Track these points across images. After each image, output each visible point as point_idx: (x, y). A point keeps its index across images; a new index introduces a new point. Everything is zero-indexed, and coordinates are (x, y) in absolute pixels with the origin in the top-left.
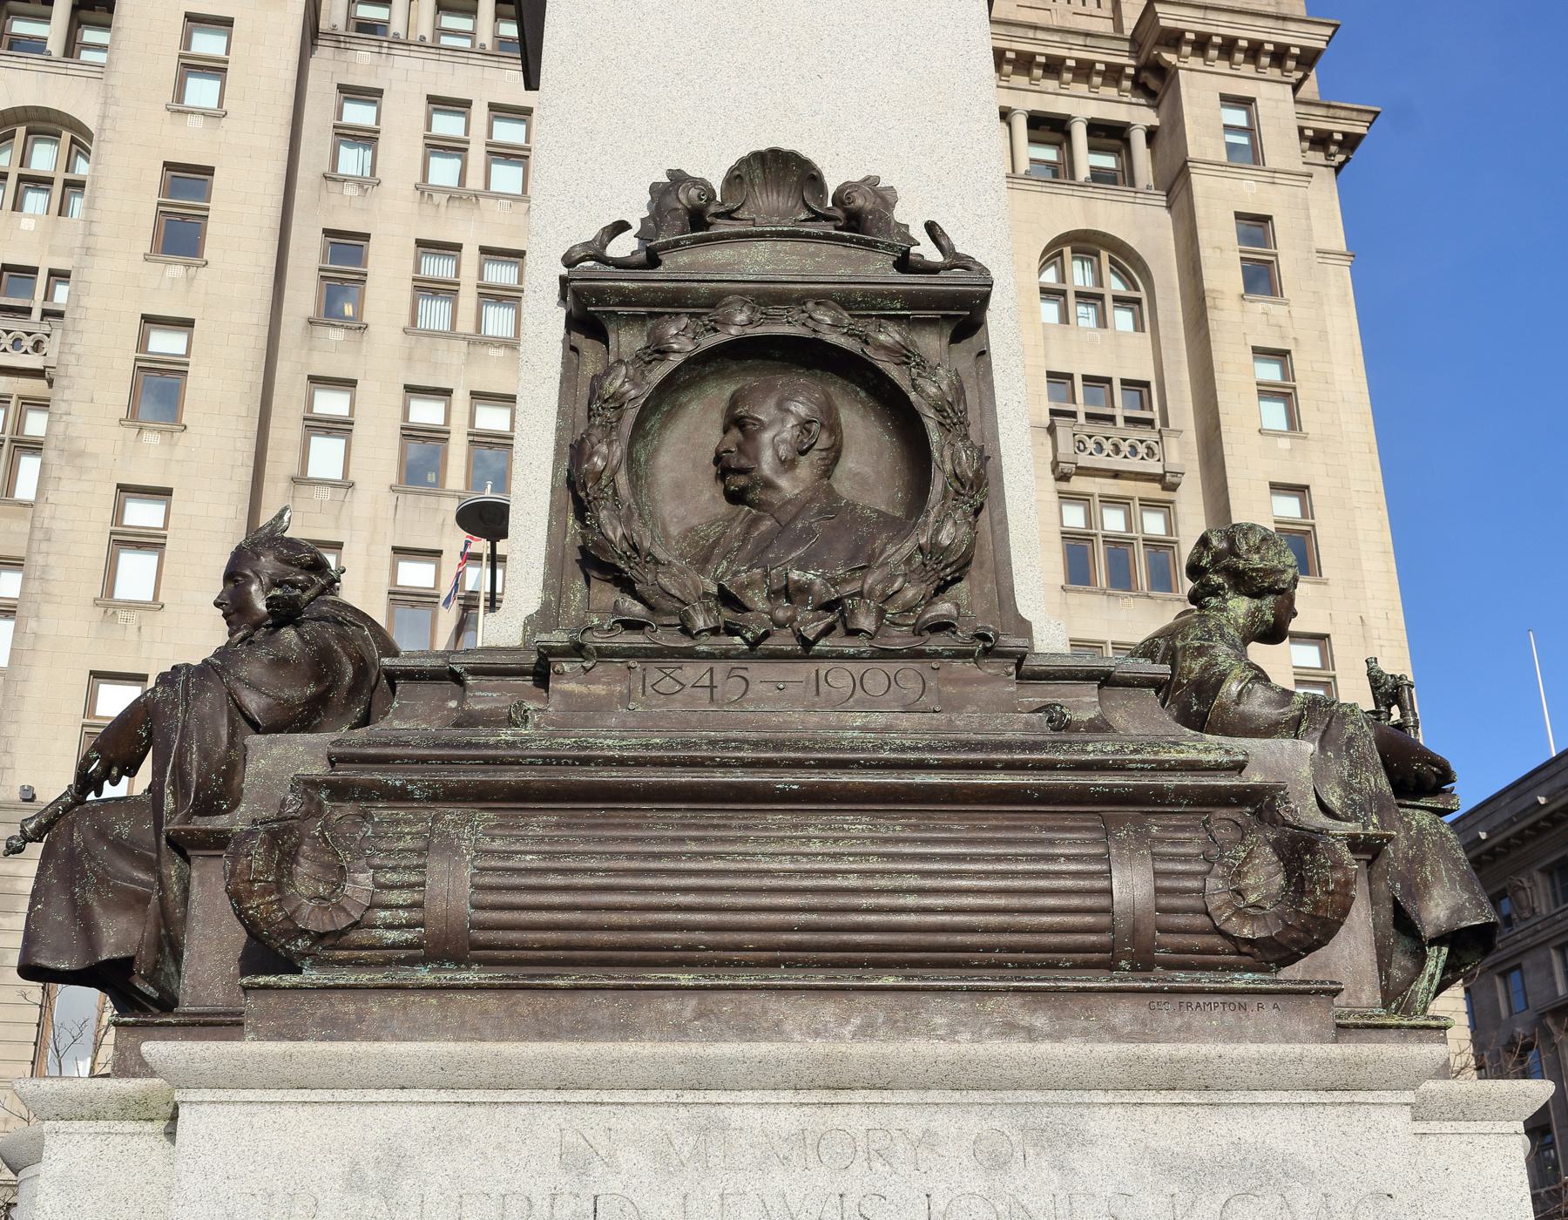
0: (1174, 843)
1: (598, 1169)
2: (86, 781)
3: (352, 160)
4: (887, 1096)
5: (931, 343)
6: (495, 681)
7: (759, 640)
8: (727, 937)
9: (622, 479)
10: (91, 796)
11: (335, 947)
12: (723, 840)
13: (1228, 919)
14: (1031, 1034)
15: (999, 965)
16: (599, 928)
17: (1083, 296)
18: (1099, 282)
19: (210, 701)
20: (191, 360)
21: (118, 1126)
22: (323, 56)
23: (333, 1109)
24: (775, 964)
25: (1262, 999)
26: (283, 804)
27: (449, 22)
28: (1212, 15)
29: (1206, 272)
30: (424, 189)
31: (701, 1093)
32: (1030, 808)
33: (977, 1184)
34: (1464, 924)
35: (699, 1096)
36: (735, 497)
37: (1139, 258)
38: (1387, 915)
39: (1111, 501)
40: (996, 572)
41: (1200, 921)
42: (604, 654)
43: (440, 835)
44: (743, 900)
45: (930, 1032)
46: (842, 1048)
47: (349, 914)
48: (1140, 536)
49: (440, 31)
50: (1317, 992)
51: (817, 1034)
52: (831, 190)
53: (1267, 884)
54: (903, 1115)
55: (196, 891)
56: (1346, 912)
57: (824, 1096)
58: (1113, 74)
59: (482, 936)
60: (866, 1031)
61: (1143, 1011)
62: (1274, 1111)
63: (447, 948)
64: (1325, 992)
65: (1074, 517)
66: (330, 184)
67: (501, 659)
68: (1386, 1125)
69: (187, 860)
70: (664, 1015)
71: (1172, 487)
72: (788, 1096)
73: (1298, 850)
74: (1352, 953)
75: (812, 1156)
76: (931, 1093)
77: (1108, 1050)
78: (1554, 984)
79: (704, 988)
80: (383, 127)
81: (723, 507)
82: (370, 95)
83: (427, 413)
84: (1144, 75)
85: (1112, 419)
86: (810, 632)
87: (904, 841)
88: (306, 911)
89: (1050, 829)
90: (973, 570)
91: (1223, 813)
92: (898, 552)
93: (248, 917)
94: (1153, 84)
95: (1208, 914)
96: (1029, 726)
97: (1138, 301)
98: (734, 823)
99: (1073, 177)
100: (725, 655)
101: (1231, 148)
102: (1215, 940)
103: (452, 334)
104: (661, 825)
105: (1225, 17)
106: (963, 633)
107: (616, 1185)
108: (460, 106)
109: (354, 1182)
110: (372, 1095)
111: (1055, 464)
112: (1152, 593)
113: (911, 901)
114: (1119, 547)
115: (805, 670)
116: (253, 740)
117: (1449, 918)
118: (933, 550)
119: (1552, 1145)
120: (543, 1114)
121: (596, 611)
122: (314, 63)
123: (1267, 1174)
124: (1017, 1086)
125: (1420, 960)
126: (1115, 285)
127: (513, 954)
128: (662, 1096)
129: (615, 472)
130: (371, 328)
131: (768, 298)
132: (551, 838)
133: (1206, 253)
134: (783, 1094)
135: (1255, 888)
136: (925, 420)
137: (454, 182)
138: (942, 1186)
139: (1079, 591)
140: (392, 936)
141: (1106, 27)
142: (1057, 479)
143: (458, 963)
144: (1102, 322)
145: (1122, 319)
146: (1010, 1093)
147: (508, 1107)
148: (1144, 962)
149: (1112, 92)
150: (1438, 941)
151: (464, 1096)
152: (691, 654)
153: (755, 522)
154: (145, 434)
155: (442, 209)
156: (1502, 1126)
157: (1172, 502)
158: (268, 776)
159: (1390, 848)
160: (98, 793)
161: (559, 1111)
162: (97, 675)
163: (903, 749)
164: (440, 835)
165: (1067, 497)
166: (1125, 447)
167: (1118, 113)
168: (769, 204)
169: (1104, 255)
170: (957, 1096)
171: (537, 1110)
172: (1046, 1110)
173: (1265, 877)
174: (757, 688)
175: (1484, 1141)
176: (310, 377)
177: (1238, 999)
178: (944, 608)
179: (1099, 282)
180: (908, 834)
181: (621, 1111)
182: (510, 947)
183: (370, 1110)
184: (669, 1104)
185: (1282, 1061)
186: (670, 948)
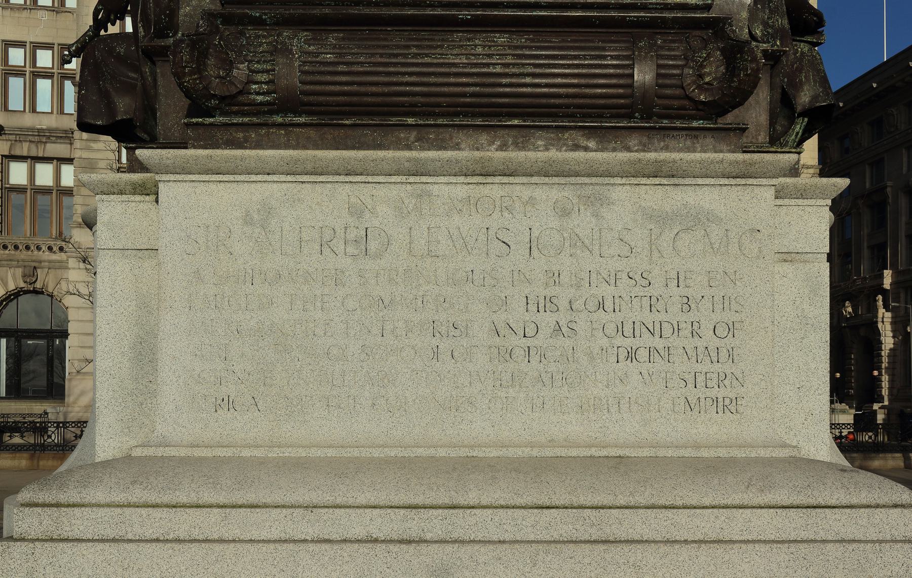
0: (670, 49)
1: (367, 215)
2: (99, 24)
4: (511, 179)
8: (433, 100)
10: (102, 33)
11: (230, 105)
12: (431, 47)
13: (694, 90)
14: (586, 149)
16: (366, 94)
21: (132, 198)
23: (234, 185)
24: (457, 114)
25: (706, 133)
26: (198, 26)
31: (418, 178)
32: (594, 30)
34: (818, 104)
38: (778, 96)
41: (678, 92)
43: (281, 43)
45: (536, 149)
46: (489, 154)
47: (236, 86)
50: (735, 129)
51: (478, 149)
53: (716, 72)
54: (520, 189)
55: (160, 82)
56: (755, 86)
59: (305, 99)
60: (503, 147)
61: (645, 140)
62: (706, 188)
63: (288, 104)
64: (740, 129)
68: (761, 195)
69: (154, 63)
70: (400, 139)
72: (462, 179)
73: (735, 51)
74: (757, 112)
75: (473, 209)
76: (534, 178)
77: (623, 156)
78: (865, 183)
79: (420, 125)
87: (526, 47)
88: (214, 85)
89: (603, 41)
91: (697, 33)
93: (185, 87)
95: (683, 88)
98: (436, 37)
102: (686, 102)
107: (376, 223)
109: (248, 220)
110: (254, 178)
113: (528, 80)
117: (810, 102)
119: (850, 262)
120: (340, 188)
123: (697, 220)
124: (577, 174)
125: (792, 122)
127: (323, 108)
132: (340, 45)
134: (459, 178)
135: (709, 74)
138: (538, 224)
140: (260, 98)
146: (573, 178)
147: (321, 184)
148: (648, 115)
150: (803, 114)
156: (821, 202)
159: (784, 59)
160: (106, 31)
161: (347, 186)
164: (281, 43)
170: (547, 180)
171: (336, 185)
172: (591, 187)
173: (714, 70)
175: (809, 209)
177: (694, 133)
180: (528, 43)
181: (377, 186)
182: (320, 104)
183: (253, 185)
184: (402, 183)
185: (712, 162)
186: (403, 106)
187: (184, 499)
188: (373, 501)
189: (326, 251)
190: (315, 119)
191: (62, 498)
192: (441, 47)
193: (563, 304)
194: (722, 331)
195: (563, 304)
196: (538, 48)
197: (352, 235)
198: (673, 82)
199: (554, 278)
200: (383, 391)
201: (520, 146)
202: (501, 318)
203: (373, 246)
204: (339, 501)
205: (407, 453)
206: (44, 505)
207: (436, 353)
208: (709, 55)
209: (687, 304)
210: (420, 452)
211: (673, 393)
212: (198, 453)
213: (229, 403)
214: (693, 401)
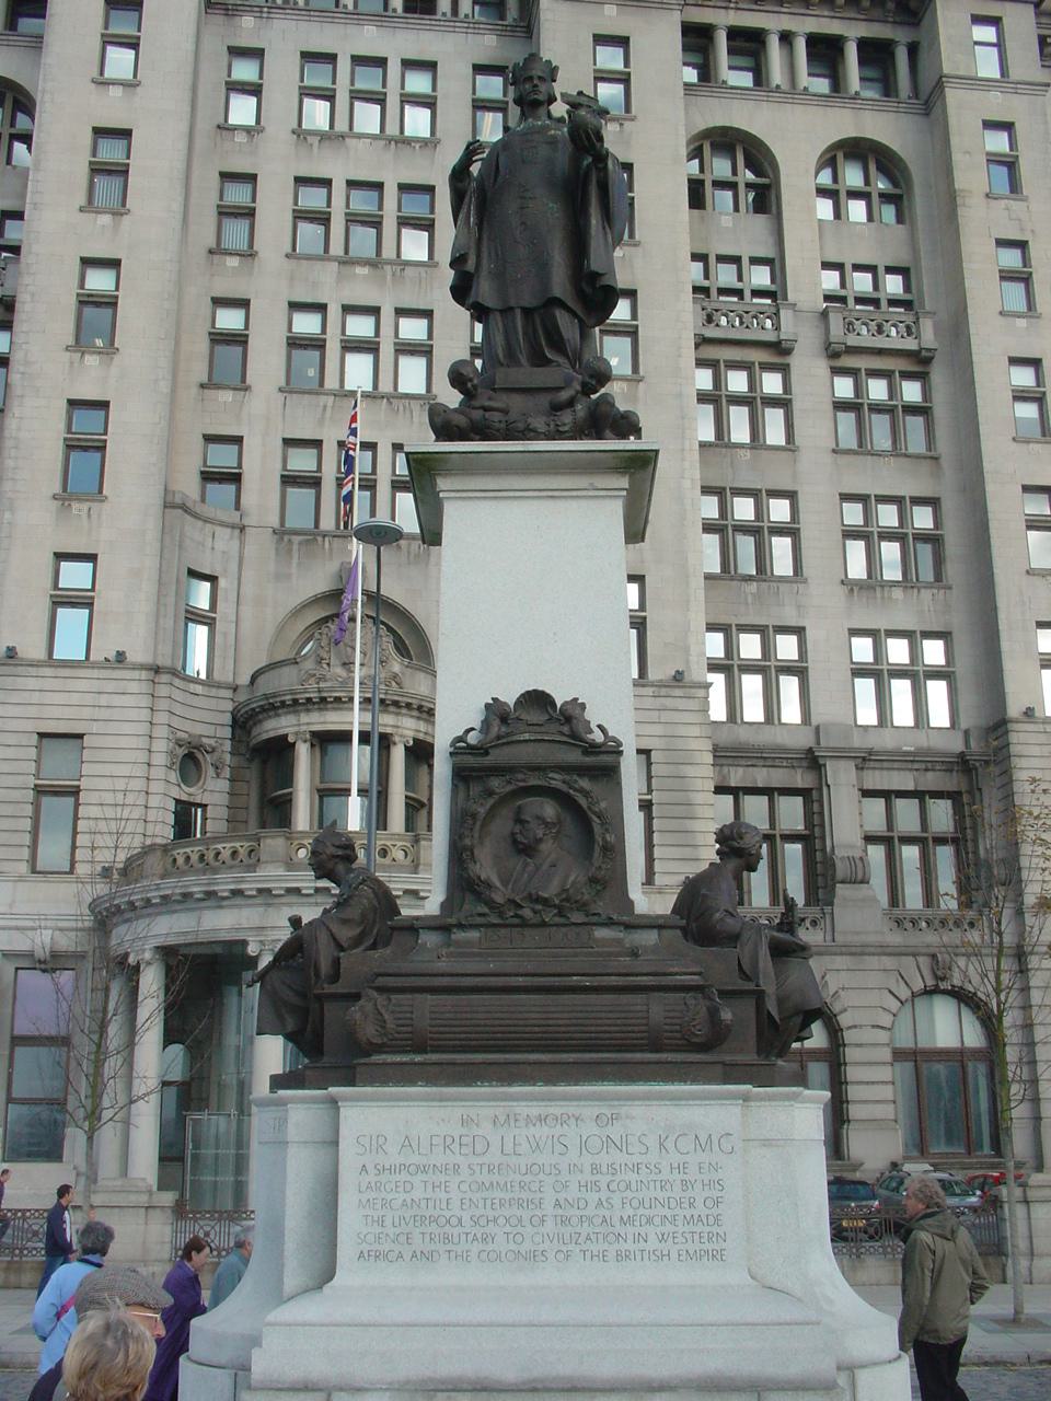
29: (956, 174)
39: (875, 373)
48: (900, 404)
52: (559, 706)
65: (844, 388)
66: (224, 132)
82: (257, 54)
106: (604, 916)
111: (828, 345)
126: (882, 185)
136: (594, 824)
152: (506, 926)
154: (87, 357)
162: (61, 557)
165: (837, 371)
168: (536, 716)
193: (604, 1186)
195: (604, 1186)
199: (595, 1169)
202: (561, 1196)
214: (691, 1252)
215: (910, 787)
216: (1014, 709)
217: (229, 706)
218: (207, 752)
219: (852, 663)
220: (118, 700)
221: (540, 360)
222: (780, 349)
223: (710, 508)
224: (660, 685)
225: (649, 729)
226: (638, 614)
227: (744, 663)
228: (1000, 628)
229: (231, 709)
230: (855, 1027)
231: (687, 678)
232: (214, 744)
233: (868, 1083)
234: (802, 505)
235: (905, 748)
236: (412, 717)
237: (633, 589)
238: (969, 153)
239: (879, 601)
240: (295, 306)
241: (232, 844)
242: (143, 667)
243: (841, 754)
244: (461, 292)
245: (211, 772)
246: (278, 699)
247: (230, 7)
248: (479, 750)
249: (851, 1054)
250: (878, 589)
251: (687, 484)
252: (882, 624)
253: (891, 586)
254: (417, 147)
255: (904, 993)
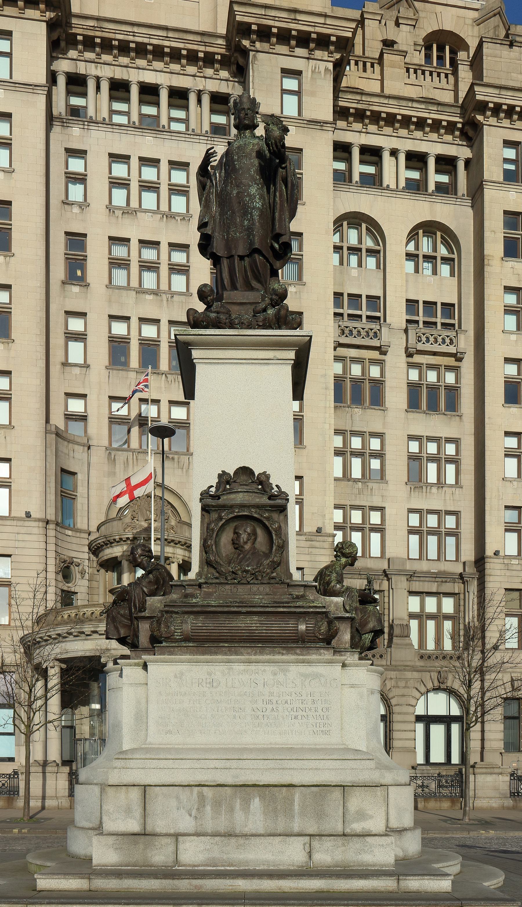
3: (76, 192)
5: (275, 516)
6: (191, 587)
7: (239, 581)
8: (233, 638)
9: (214, 547)
14: (283, 654)
15: (279, 642)
17: (427, 258)
18: (435, 249)
19: (138, 590)
20: (12, 306)
22: (57, 129)
27: (118, 106)
28: (504, 92)
29: (486, 246)
30: (111, 208)
33: (272, 678)
35: (229, 664)
36: (236, 549)
37: (455, 236)
38: (354, 630)
39: (431, 367)
40: (286, 564)
42: (211, 584)
44: (236, 631)
49: (112, 112)
57: (248, 664)
58: (451, 127)
60: (255, 654)
63: (187, 639)
65: (414, 375)
66: (66, 206)
67: (192, 583)
71: (460, 360)
72: (242, 664)
80: (88, 172)
81: (234, 550)
82: (80, 154)
83: (119, 329)
84: (466, 128)
85: (435, 324)
86: (249, 580)
90: (282, 564)
91: (319, 616)
92: (266, 562)
94: (471, 133)
96: (288, 598)
97: (453, 260)
99: (426, 190)
100: (234, 584)
101: (506, 172)
102: (316, 638)
103: (128, 288)
104: (222, 618)
105: (510, 93)
108: (125, 159)
109: (176, 676)
110: (177, 664)
111: (407, 349)
112: (446, 413)
114: (433, 389)
115: (249, 586)
116: (148, 598)
118: (273, 562)
120: (204, 667)
121: (210, 573)
122: (52, 135)
123: (317, 676)
126: (443, 251)
128: (222, 664)
129: (212, 545)
130: (91, 285)
131: (242, 506)
133: (487, 234)
137: (124, 204)
139: (413, 412)
140: (178, 637)
141: (447, 97)
142: (407, 356)
143: (189, 641)
144: (435, 272)
145: (445, 270)
148: (303, 641)
149: (449, 138)
151: (192, 664)
152: (227, 584)
153: (239, 555)
155: (120, 219)
157: (459, 367)
158: (150, 605)
163: (265, 604)
165: (411, 365)
166: (440, 340)
167: (451, 151)
168: (243, 478)
169: (439, 234)
173: (324, 628)
174: (239, 590)
176: (66, 312)
178: (274, 574)
179: (435, 249)
182: (197, 639)
187: (162, 757)
188: (216, 758)
189: (200, 686)
190: (195, 644)
191: (127, 757)
192: (236, 621)
193: (274, 702)
194: (324, 710)
195: (274, 702)
196: (267, 621)
197: (208, 681)
198: (311, 632)
199: (271, 694)
200: (218, 728)
201: (261, 653)
202: (255, 706)
203: (215, 684)
204: (206, 758)
205: (226, 747)
206: (121, 759)
207: (235, 717)
208: (322, 624)
209: (314, 702)
210: (230, 746)
211: (309, 729)
212: (161, 746)
213: (170, 732)
214: (315, 731)
215: (434, 590)
216: (489, 551)
217: (87, 542)
218: (76, 566)
219: (409, 452)
220: (27, 537)
221: (250, 288)
222: (381, 350)
223: (338, 442)
224: (310, 534)
225: (303, 557)
226: (299, 497)
227: (353, 525)
228: (486, 509)
229: (87, 543)
230: (398, 705)
231: (323, 531)
232: (80, 562)
233: (403, 731)
234: (387, 442)
235: (432, 571)
236: (181, 549)
237: (297, 483)
238: (494, 231)
239: (424, 494)
240: (113, 317)
241: (92, 609)
242: (39, 520)
243: (400, 573)
244: (205, 247)
245: (78, 576)
246: (112, 538)
247: (65, 120)
248: (216, 497)
249: (396, 717)
250: (424, 488)
251: (327, 426)
252: (424, 506)
253: (431, 486)
254: (179, 220)
255: (423, 689)
